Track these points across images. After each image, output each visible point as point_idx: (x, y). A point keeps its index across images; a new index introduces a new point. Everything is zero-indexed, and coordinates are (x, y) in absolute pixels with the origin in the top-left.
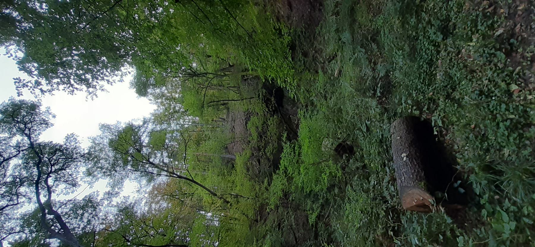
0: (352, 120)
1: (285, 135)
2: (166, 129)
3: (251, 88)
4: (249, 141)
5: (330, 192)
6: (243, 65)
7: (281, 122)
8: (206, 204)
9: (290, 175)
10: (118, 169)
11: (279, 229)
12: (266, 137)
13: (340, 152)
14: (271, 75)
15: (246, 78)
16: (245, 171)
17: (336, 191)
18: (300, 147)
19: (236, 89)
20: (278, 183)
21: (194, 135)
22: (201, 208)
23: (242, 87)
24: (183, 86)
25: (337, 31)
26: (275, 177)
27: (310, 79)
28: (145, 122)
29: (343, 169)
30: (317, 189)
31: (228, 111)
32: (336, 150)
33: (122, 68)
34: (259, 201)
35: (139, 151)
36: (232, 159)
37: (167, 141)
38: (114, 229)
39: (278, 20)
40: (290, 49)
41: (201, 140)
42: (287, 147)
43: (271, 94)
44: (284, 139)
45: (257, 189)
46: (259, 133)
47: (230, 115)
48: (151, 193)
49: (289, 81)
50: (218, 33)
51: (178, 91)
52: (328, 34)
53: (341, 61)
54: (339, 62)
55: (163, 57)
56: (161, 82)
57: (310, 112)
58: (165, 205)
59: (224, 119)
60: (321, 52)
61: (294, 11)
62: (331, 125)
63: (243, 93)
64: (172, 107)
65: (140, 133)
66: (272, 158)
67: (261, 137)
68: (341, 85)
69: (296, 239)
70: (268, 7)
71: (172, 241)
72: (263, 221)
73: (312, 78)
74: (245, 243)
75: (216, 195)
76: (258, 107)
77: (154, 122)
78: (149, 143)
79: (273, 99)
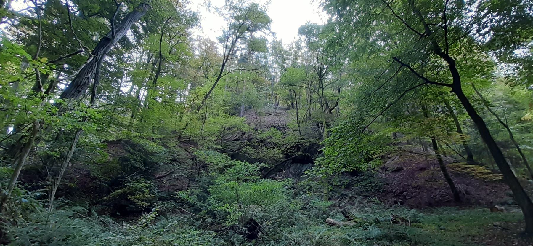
0: (283, 238)
1: (266, 166)
2: (268, 52)
3: (310, 131)
4: (257, 130)
5: (207, 213)
6: (332, 123)
7: (277, 162)
8: (197, 90)
9: (226, 170)
10: (232, 12)
11: (171, 160)
12: (261, 147)
13: (250, 224)
14: (326, 150)
15: (320, 126)
16: (228, 126)
17: (210, 220)
18: (254, 181)
19: (308, 116)
20: (218, 159)
21: (262, 78)
22: (193, 85)
23: (311, 122)
24: (309, 67)
25: (377, 221)
26: (224, 155)
27: (322, 192)
28: (274, 34)
29: (232, 228)
30: (211, 199)
31: (286, 109)
32: (251, 220)
33: (325, 12)
34: (200, 140)
35: (248, 29)
36: (240, 113)
37: (256, 53)
38: (178, 9)
39: (382, 157)
40: (353, 170)
41: (258, 84)
42: (254, 167)
43: (305, 151)
44: (262, 165)
45: (211, 138)
46: (265, 140)
47: (282, 111)
48: (208, 41)
49: (321, 169)
50: (366, 98)
51: (304, 62)
52: (371, 211)
53: (346, 226)
54: (342, 223)
55: (337, 48)
56: (312, 47)
57: (288, 191)
58: (197, 53)
59: (278, 105)
60: (351, 204)
61: (392, 175)
62: (276, 215)
63: (304, 123)
64: (289, 57)
65: (264, 30)
66: (241, 152)
67: (262, 142)
68: (318, 225)
69: (161, 177)
70: (394, 148)
71: (164, 59)
72: (179, 144)
73: (323, 194)
74: (158, 127)
75: (206, 98)
76: (291, 138)
77: (274, 41)
78: (255, 38)
79: (299, 153)
